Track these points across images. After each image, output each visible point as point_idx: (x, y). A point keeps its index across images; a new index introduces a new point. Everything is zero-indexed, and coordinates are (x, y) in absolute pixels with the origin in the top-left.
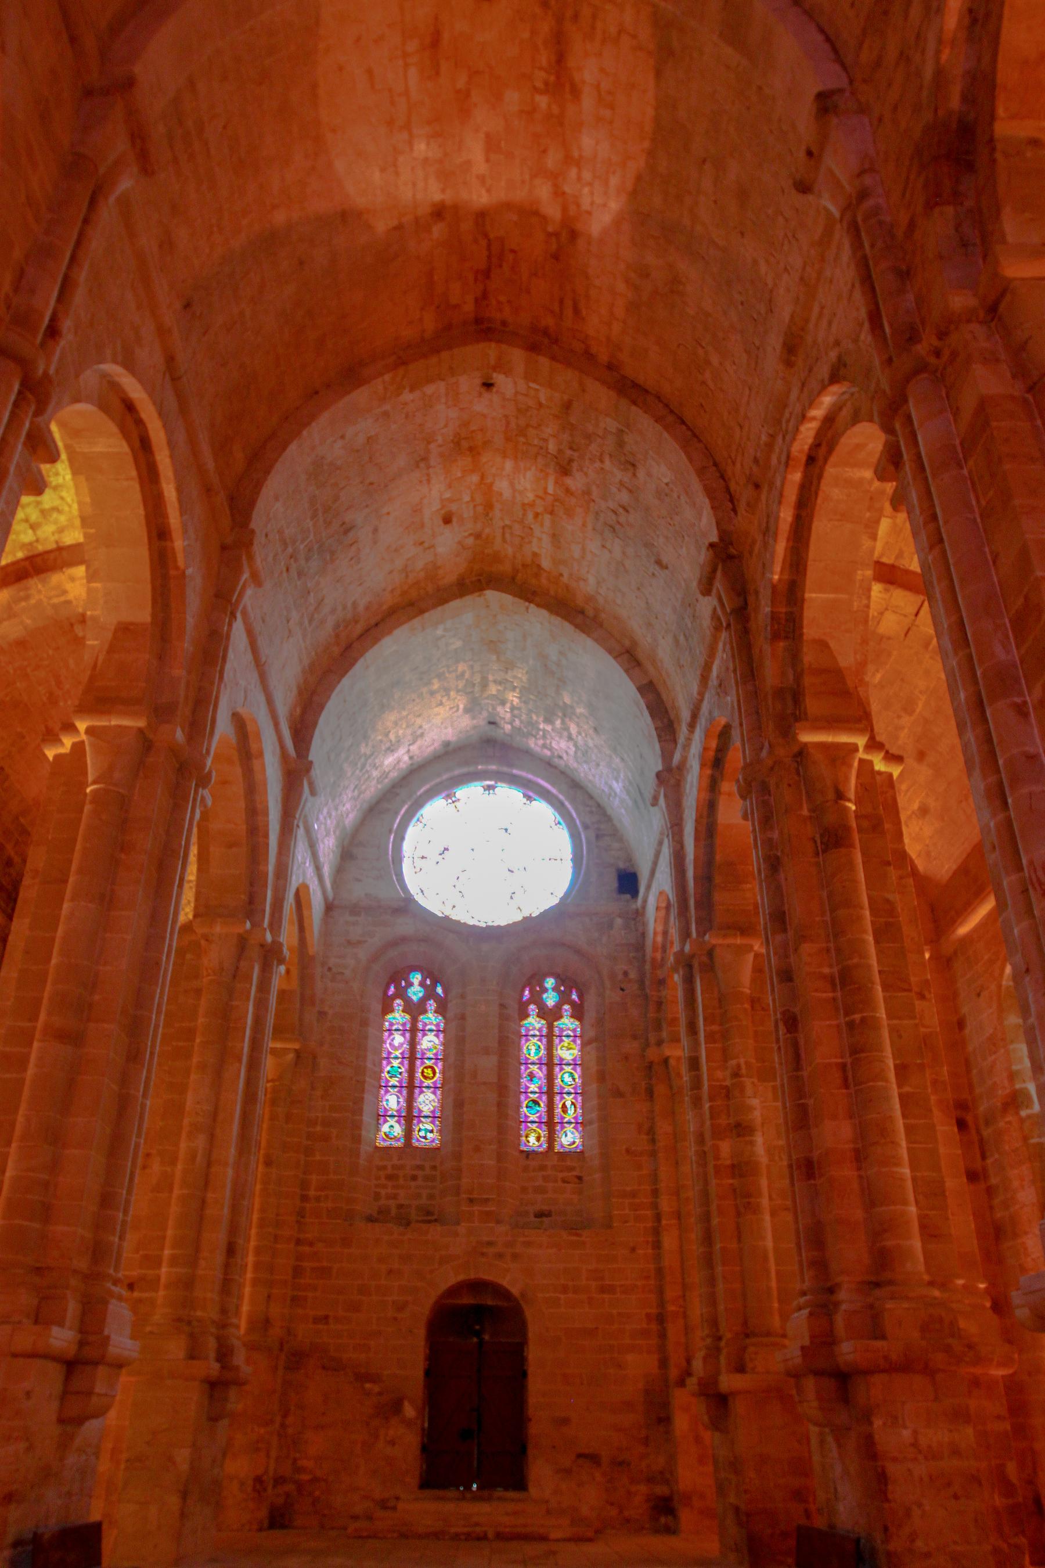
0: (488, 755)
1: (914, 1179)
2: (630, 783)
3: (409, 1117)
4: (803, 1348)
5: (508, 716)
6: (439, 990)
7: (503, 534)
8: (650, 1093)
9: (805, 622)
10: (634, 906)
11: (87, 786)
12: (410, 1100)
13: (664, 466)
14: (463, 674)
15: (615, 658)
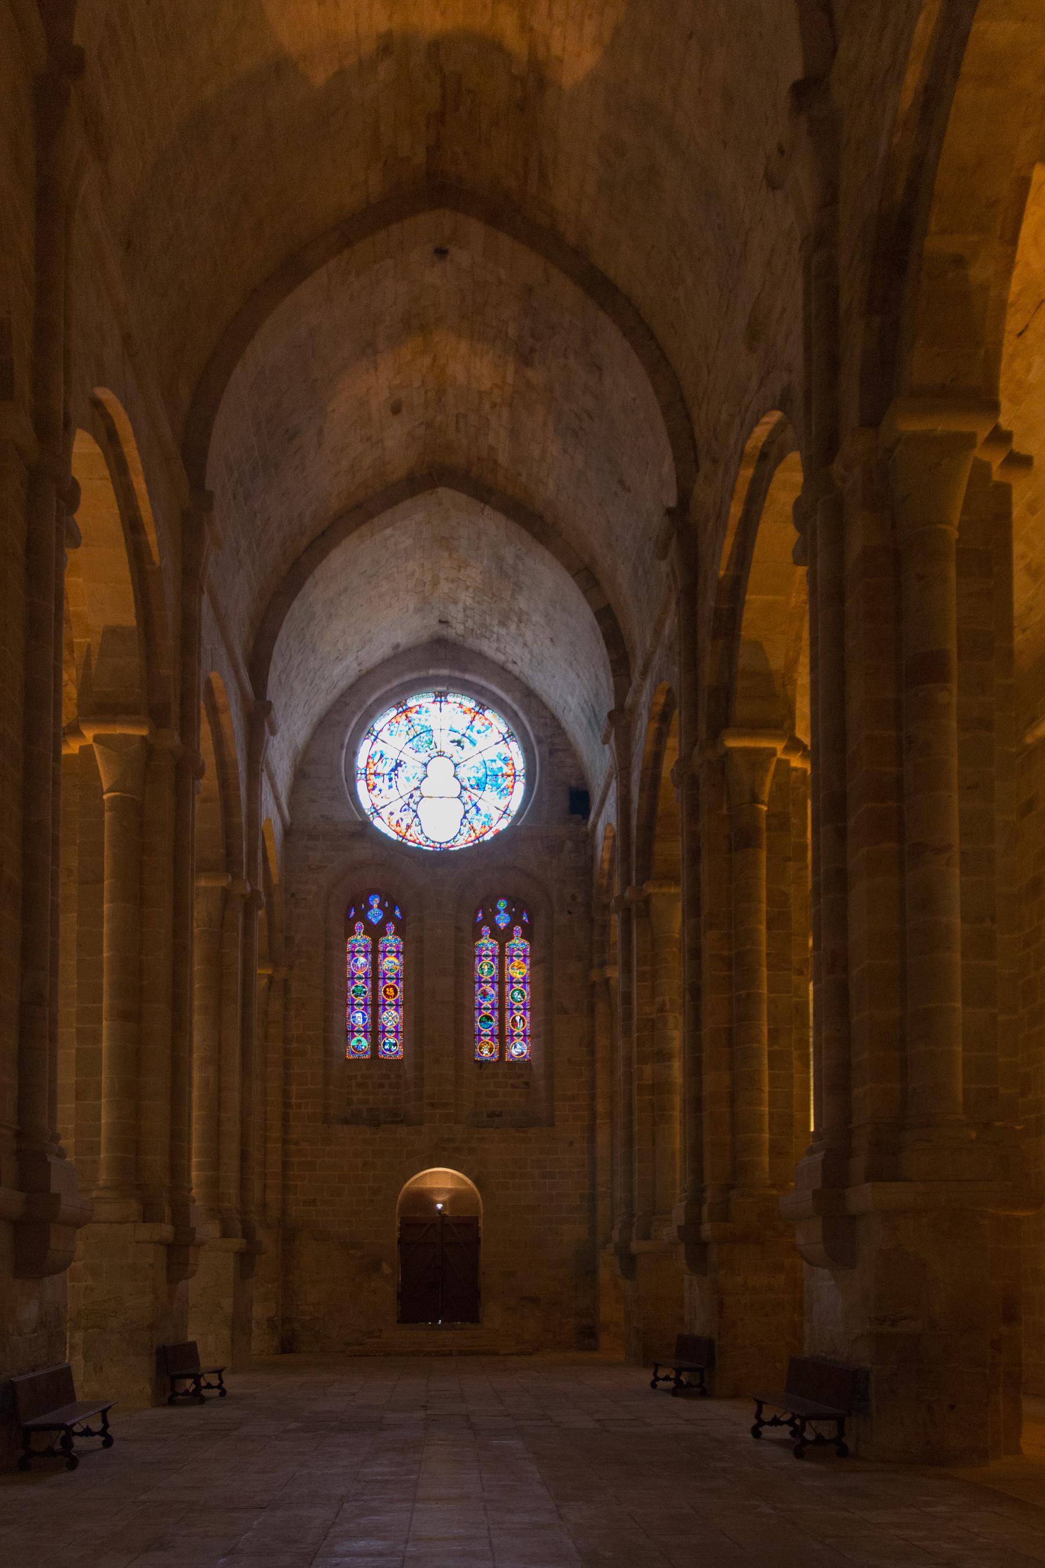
0: (443, 661)
1: (771, 1114)
2: (585, 701)
3: (375, 1032)
4: (679, 1227)
5: (461, 616)
6: (397, 913)
7: (457, 422)
8: (592, 1010)
9: (744, 624)
10: (584, 829)
11: (103, 794)
12: (375, 1017)
13: (628, 384)
14: (413, 574)
15: (573, 576)
